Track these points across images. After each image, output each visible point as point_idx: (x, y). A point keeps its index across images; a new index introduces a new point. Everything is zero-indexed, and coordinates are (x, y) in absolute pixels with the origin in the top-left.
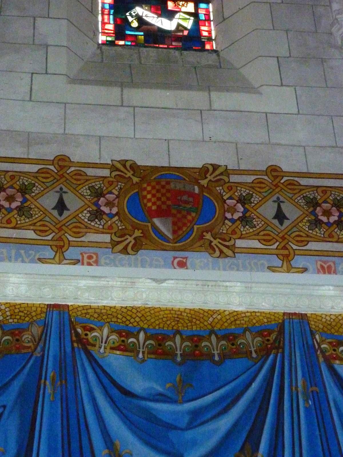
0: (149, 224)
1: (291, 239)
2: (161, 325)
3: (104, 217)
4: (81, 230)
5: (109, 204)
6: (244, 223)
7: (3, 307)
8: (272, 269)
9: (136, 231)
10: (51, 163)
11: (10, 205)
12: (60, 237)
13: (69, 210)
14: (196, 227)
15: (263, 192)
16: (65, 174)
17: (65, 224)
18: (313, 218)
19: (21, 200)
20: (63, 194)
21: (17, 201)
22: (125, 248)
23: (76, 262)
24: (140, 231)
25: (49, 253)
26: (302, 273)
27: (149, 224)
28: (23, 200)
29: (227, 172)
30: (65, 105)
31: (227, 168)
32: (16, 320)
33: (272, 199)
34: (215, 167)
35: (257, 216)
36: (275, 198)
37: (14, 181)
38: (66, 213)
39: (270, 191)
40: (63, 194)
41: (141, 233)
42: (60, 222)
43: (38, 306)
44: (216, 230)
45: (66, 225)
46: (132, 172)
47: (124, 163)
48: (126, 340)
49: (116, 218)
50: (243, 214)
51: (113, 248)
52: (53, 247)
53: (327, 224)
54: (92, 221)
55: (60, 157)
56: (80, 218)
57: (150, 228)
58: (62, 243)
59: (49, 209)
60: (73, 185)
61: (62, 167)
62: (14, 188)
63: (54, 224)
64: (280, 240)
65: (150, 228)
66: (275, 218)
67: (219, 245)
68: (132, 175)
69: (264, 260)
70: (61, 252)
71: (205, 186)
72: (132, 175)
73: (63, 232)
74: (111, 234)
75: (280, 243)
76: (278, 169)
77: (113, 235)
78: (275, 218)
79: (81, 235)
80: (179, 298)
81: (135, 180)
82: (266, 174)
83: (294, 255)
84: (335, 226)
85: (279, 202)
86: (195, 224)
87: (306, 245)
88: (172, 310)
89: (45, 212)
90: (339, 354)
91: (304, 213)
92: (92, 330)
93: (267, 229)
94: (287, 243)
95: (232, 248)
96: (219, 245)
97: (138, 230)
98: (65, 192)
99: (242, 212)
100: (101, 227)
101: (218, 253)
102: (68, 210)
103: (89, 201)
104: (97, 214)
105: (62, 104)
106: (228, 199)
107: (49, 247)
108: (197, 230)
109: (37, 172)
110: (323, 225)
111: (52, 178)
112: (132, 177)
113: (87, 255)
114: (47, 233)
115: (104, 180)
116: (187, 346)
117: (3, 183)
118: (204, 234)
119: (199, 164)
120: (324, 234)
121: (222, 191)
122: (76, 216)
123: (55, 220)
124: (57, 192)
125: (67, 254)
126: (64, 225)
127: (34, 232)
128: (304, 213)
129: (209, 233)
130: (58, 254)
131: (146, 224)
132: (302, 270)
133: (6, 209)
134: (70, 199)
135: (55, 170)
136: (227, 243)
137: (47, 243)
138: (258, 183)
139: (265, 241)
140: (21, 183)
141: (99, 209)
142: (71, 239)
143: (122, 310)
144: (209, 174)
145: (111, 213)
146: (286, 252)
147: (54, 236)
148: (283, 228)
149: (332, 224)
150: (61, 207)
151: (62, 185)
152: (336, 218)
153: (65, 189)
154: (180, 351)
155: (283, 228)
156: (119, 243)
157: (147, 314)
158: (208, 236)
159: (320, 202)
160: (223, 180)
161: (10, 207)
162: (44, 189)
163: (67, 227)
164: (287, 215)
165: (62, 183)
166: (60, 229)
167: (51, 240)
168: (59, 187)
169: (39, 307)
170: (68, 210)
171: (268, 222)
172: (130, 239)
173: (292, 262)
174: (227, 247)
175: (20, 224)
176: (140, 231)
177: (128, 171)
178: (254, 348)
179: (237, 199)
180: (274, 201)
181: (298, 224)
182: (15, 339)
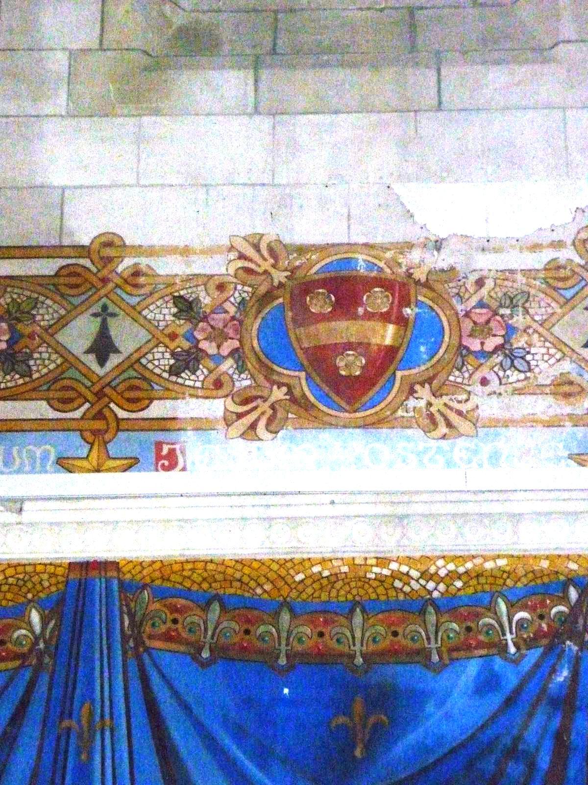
1: (114, 395)
5: (218, 336)
8: (65, 464)
13: (85, 353)
14: (399, 374)
15: (70, 296)
17: (110, 382)
20: (109, 319)
21: (495, 335)
22: (253, 426)
23: (131, 464)
24: (284, 389)
25: (76, 445)
26: (125, 471)
33: (91, 311)
35: (55, 350)
36: (97, 308)
38: (114, 360)
40: (109, 319)
41: (286, 394)
42: (101, 378)
46: (272, 261)
48: (473, 625)
49: (230, 362)
50: (7, 343)
52: (85, 434)
54: (178, 375)
55: (103, 239)
56: (144, 366)
66: (88, 351)
68: (274, 266)
69: (50, 447)
70: (101, 442)
78: (88, 351)
79: (140, 405)
86: (397, 369)
89: (69, 361)
90: (255, 641)
91: (52, 335)
98: (113, 315)
99: (7, 341)
107: (78, 433)
109: (57, 275)
113: (169, 446)
114: (76, 404)
120: (203, 382)
124: (95, 315)
125: (112, 449)
126: (109, 384)
127: (49, 404)
129: (427, 386)
130: (96, 447)
131: (297, 373)
132: (126, 462)
137: (74, 425)
141: (196, 347)
142: (122, 414)
145: (219, 354)
146: (99, 425)
147: (88, 409)
151: (104, 300)
161: (482, 349)
164: (117, 343)
165: (106, 296)
166: (100, 395)
167: (82, 418)
168: (100, 303)
171: (72, 360)
172: (265, 407)
173: (109, 446)
174: (459, 413)
175: (22, 384)
176: (284, 389)
177: (265, 260)
178: (511, 633)
180: (95, 315)
182: (243, 629)
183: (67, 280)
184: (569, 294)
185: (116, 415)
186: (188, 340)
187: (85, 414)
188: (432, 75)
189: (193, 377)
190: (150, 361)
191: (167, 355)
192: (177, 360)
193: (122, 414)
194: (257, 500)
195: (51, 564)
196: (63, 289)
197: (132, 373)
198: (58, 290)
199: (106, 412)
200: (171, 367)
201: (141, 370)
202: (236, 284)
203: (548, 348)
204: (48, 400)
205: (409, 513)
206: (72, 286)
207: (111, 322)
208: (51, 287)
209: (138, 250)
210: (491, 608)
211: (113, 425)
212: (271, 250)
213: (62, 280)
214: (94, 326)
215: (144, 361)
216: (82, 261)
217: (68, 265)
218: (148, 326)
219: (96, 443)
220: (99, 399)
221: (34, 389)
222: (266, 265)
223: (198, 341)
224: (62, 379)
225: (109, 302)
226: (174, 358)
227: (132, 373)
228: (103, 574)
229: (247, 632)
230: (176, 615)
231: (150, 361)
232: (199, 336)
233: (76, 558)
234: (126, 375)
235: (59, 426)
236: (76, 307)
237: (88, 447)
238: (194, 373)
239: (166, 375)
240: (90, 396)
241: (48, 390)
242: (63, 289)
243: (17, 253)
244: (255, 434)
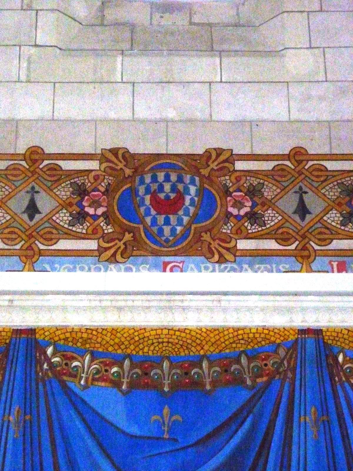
0: (141, 226)
2: (146, 350)
3: (88, 218)
4: (53, 236)
6: (252, 221)
7: (3, 334)
9: (127, 233)
10: (21, 157)
11: (239, 212)
12: (30, 246)
16: (37, 170)
18: (78, 210)
19: (249, 204)
20: (35, 194)
21: (246, 206)
24: (132, 234)
27: (141, 226)
28: (252, 204)
29: (232, 158)
30: (210, 85)
31: (232, 152)
32: (232, 350)
33: (293, 190)
34: (219, 152)
35: (277, 212)
37: (99, 181)
39: (292, 179)
42: (30, 227)
43: (340, 331)
44: (215, 231)
45: (310, 231)
47: (114, 151)
51: (100, 256)
53: (236, 217)
54: (73, 226)
57: (142, 230)
58: (306, 253)
59: (19, 212)
60: (45, 182)
61: (35, 161)
62: (99, 191)
63: (24, 230)
64: (300, 239)
65: (142, 230)
66: (295, 212)
67: (220, 249)
71: (207, 175)
72: (125, 166)
73: (307, 240)
74: (99, 239)
75: (300, 242)
76: (303, 151)
77: (101, 240)
78: (295, 212)
80: (344, 316)
81: (128, 172)
82: (25, 158)
83: (316, 256)
84: (246, 218)
85: (301, 192)
87: (55, 243)
88: (57, 330)
92: (74, 358)
93: (284, 225)
94: (308, 242)
95: (233, 251)
96: (116, 247)
97: (129, 233)
98: (37, 192)
100: (229, 232)
101: (216, 257)
102: (40, 213)
103: (333, 201)
104: (81, 216)
105: (49, 84)
106: (235, 191)
108: (195, 230)
110: (88, 218)
111: (290, 176)
112: (124, 168)
115: (88, 174)
116: (137, 373)
117: (227, 186)
118: (202, 234)
119: (200, 151)
121: (87, 181)
122: (49, 219)
123: (26, 226)
127: (276, 241)
128: (329, 205)
129: (209, 233)
133: (91, 216)
134: (312, 201)
135: (25, 165)
136: (228, 245)
138: (279, 170)
139: (284, 239)
140: (107, 184)
142: (317, 247)
143: (274, 331)
144: (211, 161)
146: (30, 253)
147: (298, 245)
148: (32, 223)
149: (99, 217)
150: (302, 210)
152: (248, 209)
153: (37, 188)
154: (128, 378)
155: (32, 223)
156: (106, 249)
157: (239, 336)
158: (206, 237)
159: (89, 190)
160: (105, 168)
162: (13, 190)
163: (311, 233)
166: (30, 236)
169: (257, 333)
170: (40, 213)
172: (121, 244)
176: (132, 234)
177: (121, 162)
179: (246, 190)
181: (322, 218)
183: (12, 172)
184: (285, 184)
185: (313, 248)
186: (78, 207)
187: (297, 247)
188: (218, 60)
189: (81, 227)
190: (57, 218)
191: (68, 215)
192: (344, 217)
193: (317, 247)
194: (144, 297)
195: (172, 330)
196: (11, 178)
197: (47, 225)
198: (7, 177)
199: (33, 246)
200: (70, 221)
201: (53, 223)
202: (104, 176)
203: (274, 214)
204: (276, 239)
205: (150, 305)
206: (15, 176)
207: (36, 196)
208: (271, 177)
209: (51, 156)
210: (238, 361)
211: (313, 254)
212: (124, 157)
213: (9, 172)
214: (28, 198)
215: (54, 218)
216: (21, 162)
217: (14, 164)
218: (57, 198)
219: (28, 263)
220: (30, 239)
221: (268, 234)
222: (121, 166)
223: (84, 207)
224: (283, 228)
225: (35, 185)
226: (342, 217)
227: (47, 225)
228: (18, 336)
229: (106, 371)
230: (265, 362)
231: (57, 218)
232: (85, 204)
233: (29, 326)
234: (316, 226)
235: (8, 253)
236: (17, 187)
237: (300, 265)
238: (82, 225)
239: (338, 226)
240: (24, 236)
241: (275, 233)
242: (11, 178)
243: (260, 158)
244: (115, 259)
